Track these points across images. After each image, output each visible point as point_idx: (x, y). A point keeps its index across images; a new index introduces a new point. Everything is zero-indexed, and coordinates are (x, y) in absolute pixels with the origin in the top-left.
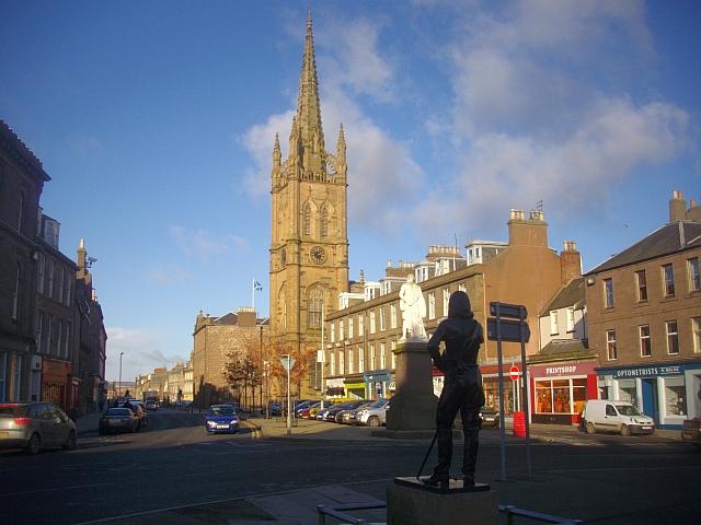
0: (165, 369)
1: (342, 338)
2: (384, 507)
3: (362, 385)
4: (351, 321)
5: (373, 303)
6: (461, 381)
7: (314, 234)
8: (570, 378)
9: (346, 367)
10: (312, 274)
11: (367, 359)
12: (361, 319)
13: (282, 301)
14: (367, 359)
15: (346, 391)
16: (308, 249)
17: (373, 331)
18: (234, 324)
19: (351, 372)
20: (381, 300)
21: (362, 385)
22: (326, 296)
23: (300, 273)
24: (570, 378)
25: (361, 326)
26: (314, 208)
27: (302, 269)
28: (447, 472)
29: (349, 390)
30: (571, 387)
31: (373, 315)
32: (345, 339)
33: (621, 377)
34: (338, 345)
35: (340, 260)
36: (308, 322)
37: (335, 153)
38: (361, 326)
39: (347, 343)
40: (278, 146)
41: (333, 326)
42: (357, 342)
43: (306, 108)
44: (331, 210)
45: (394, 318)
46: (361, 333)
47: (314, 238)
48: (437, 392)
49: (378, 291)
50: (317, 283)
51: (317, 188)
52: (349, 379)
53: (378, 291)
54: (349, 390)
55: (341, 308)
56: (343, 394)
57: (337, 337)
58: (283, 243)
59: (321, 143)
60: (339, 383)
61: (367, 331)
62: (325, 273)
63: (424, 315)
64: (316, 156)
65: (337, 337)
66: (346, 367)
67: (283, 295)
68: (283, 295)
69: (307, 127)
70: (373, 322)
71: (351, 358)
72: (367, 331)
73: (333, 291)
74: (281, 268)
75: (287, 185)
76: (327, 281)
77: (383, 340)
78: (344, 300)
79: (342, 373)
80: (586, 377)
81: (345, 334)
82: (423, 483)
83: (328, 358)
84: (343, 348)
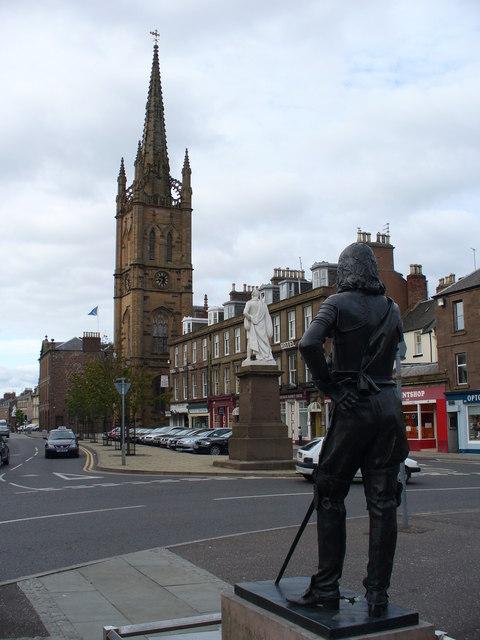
0: (14, 394)
2: (218, 622)
6: (365, 414)
8: (418, 402)
10: (158, 300)
20: (225, 324)
23: (145, 298)
24: (418, 402)
26: (158, 234)
28: (335, 586)
30: (419, 412)
33: (468, 402)
39: (190, 368)
44: (175, 235)
45: (238, 342)
48: (359, 471)
49: (221, 315)
59: (167, 168)
61: (210, 356)
62: (169, 298)
66: (189, 392)
72: (210, 356)
73: (177, 317)
80: (434, 401)
82: (284, 605)
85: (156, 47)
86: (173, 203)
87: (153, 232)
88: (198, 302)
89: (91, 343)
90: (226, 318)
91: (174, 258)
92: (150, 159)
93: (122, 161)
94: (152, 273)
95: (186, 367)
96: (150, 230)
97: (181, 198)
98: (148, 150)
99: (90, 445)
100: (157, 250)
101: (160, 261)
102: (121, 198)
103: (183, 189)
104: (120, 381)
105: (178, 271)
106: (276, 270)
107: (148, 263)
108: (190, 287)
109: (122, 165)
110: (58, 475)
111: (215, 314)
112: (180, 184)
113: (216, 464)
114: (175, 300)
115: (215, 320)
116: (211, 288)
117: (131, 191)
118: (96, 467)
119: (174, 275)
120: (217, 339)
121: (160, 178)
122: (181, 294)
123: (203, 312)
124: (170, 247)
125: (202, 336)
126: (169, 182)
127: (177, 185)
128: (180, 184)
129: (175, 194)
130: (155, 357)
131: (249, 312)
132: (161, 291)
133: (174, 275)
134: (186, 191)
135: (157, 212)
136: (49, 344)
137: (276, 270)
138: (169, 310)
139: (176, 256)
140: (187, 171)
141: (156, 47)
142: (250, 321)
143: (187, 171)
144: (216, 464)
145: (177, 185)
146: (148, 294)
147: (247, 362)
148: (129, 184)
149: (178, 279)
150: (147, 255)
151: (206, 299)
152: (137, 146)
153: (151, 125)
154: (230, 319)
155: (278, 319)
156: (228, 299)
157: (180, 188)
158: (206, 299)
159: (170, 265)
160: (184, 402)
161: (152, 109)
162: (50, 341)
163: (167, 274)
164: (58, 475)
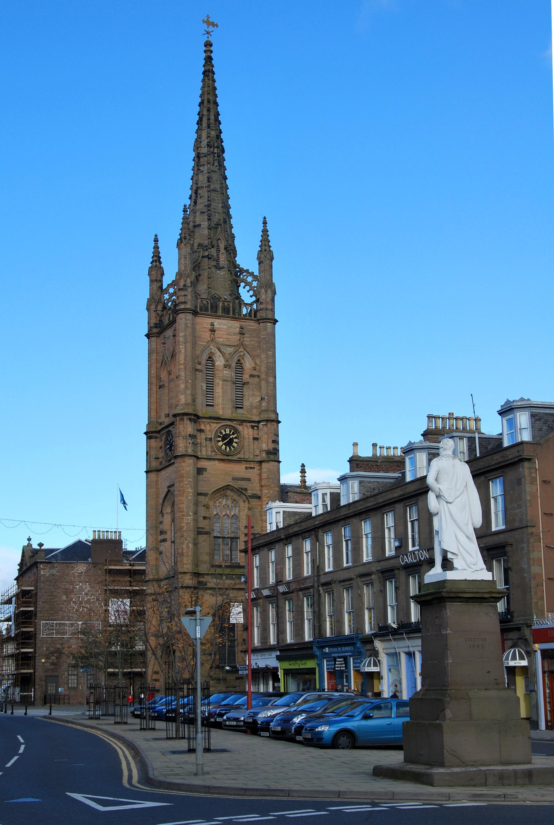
1: (272, 580)
3: (310, 664)
4: (289, 551)
5: (328, 518)
7: (223, 406)
9: (280, 632)
10: (218, 473)
11: (318, 618)
12: (366, 528)
13: (167, 519)
14: (318, 618)
15: (280, 674)
16: (210, 429)
17: (328, 567)
18: (85, 559)
19: (289, 639)
20: (343, 512)
21: (310, 664)
22: (242, 510)
25: (306, 560)
26: (220, 362)
27: (203, 464)
29: (287, 672)
31: (328, 539)
32: (279, 582)
34: (266, 592)
35: (264, 447)
36: (212, 555)
37: (254, 268)
38: (306, 560)
39: (282, 589)
40: (157, 258)
41: (257, 561)
42: (300, 588)
43: (203, 192)
44: (248, 364)
46: (307, 571)
47: (220, 412)
48: (19, 737)
49: (335, 497)
50: (227, 487)
51: (225, 327)
52: (286, 652)
53: (335, 497)
54: (287, 672)
55: (271, 527)
56: (276, 679)
57: (264, 577)
58: (167, 421)
59: (231, 251)
60: (268, 661)
61: (317, 567)
62: (239, 470)
63: (479, 522)
64: (222, 273)
65: (264, 577)
66: (280, 632)
67: (168, 509)
68: (168, 509)
69: (205, 224)
70: (328, 554)
71: (288, 616)
72: (317, 567)
73: (254, 502)
74: (165, 464)
75: (174, 321)
76: (244, 484)
77: (388, 573)
78: (275, 516)
79: (272, 641)
81: (279, 573)
83: (247, 613)
84: (275, 597)
85: (208, 44)
86: (244, 311)
87: (210, 359)
88: (289, 477)
89: (100, 552)
90: (343, 502)
91: (246, 403)
92: (202, 234)
93: (156, 240)
94: (210, 428)
95: (274, 588)
96: (205, 356)
97: (257, 301)
98: (198, 220)
99: (118, 730)
100: (218, 390)
101: (223, 406)
102: (155, 303)
103: (260, 286)
104: (193, 613)
105: (255, 424)
106: (430, 417)
107: (202, 411)
108: (276, 452)
109: (156, 248)
110: (78, 797)
111: (324, 495)
112: (255, 278)
113: (380, 772)
114: (253, 474)
115: (325, 506)
116: (315, 455)
117: (171, 290)
118: (146, 779)
119: (247, 432)
120: (389, 520)
121: (218, 267)
122: (261, 462)
123: (303, 492)
124: (239, 385)
125: (302, 534)
126: (236, 274)
127: (250, 279)
128: (255, 278)
129: (246, 295)
130: (219, 571)
131: (436, 480)
132: (227, 459)
133: (247, 432)
134: (266, 286)
135: (216, 325)
136: (36, 552)
137: (430, 417)
138: (241, 491)
139: (251, 399)
140: (265, 255)
141: (208, 44)
142: (438, 497)
143: (265, 255)
144: (380, 772)
145: (250, 279)
146: (203, 464)
147: (435, 574)
148: (167, 280)
149: (255, 439)
150: (201, 400)
151: (303, 471)
152: (182, 215)
153: (203, 179)
154: (349, 505)
155: (496, 489)
156: (346, 469)
157: (255, 284)
158: (303, 471)
159: (241, 414)
160: (271, 649)
161: (204, 150)
162: (35, 546)
163: (236, 431)
164: (78, 797)
